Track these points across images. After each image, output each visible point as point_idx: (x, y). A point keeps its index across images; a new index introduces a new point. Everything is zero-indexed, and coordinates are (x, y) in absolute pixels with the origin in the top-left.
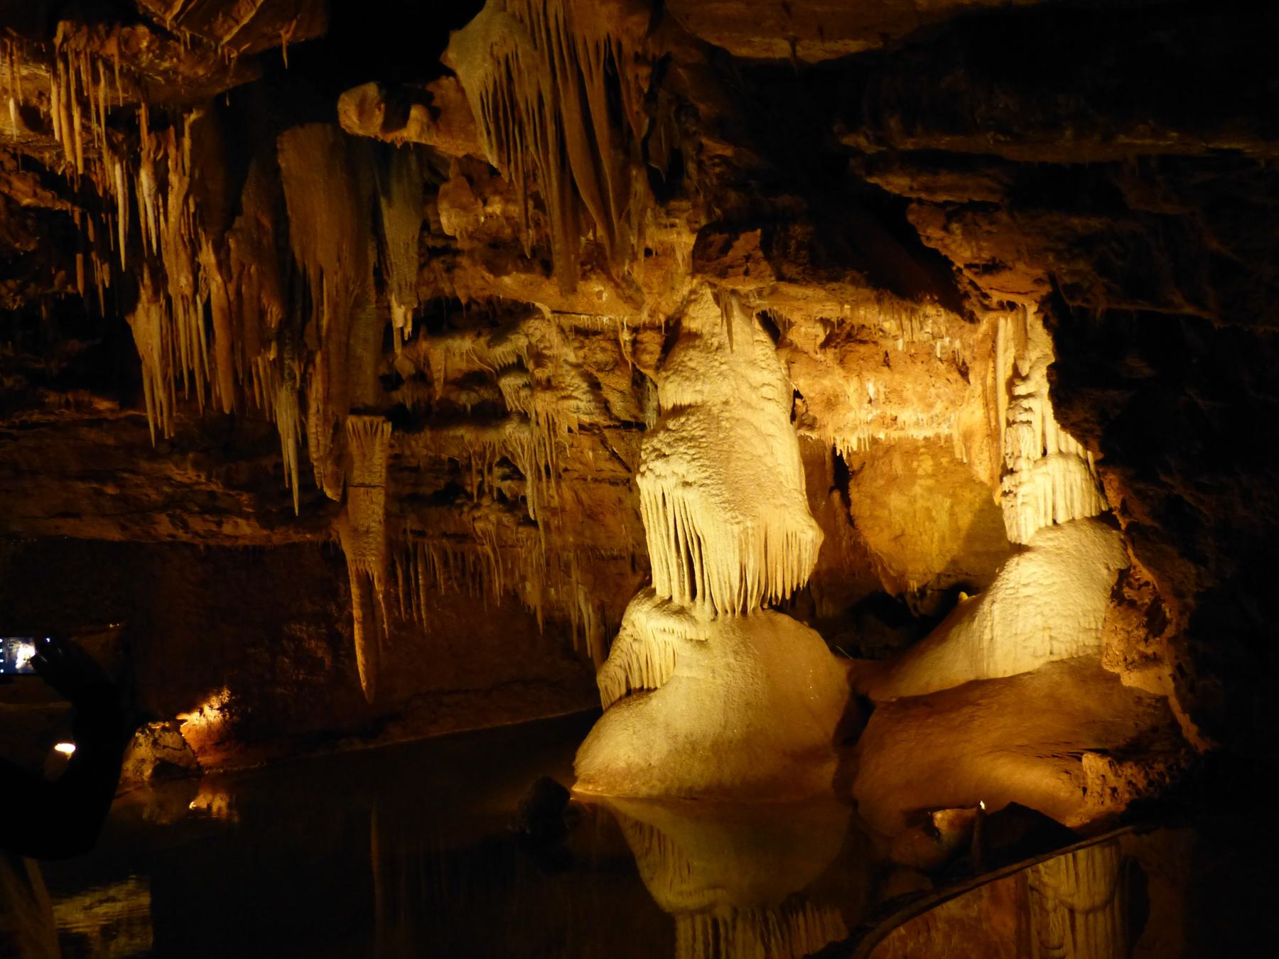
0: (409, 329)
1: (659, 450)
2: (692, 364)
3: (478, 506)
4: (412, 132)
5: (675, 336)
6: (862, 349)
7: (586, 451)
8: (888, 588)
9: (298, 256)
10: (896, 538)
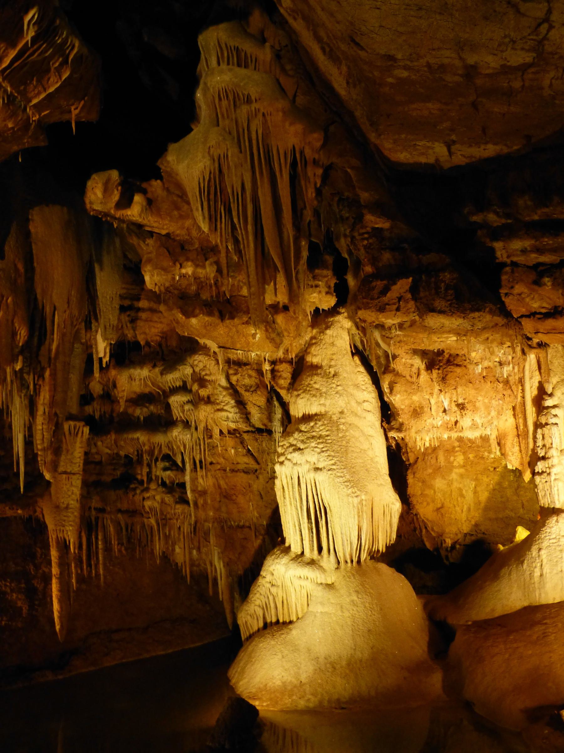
0: (107, 359)
1: (295, 445)
2: (316, 386)
3: (147, 489)
4: (135, 211)
5: (301, 369)
6: (458, 370)
7: (229, 449)
8: (428, 545)
9: (39, 297)
10: (438, 509)
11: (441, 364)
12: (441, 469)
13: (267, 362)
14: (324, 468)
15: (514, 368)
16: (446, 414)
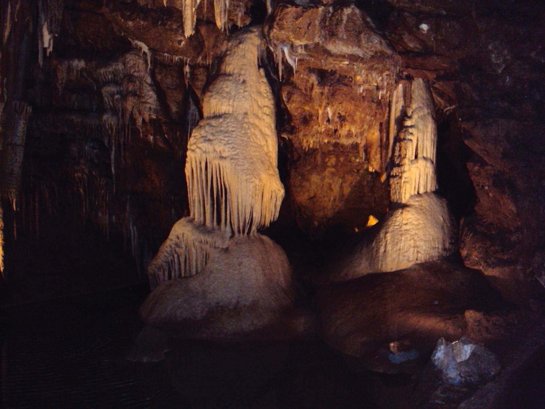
0: (51, 49)
2: (227, 90)
6: (345, 89)
10: (311, 198)
12: (318, 167)
14: (228, 157)
15: (387, 93)
16: (329, 124)
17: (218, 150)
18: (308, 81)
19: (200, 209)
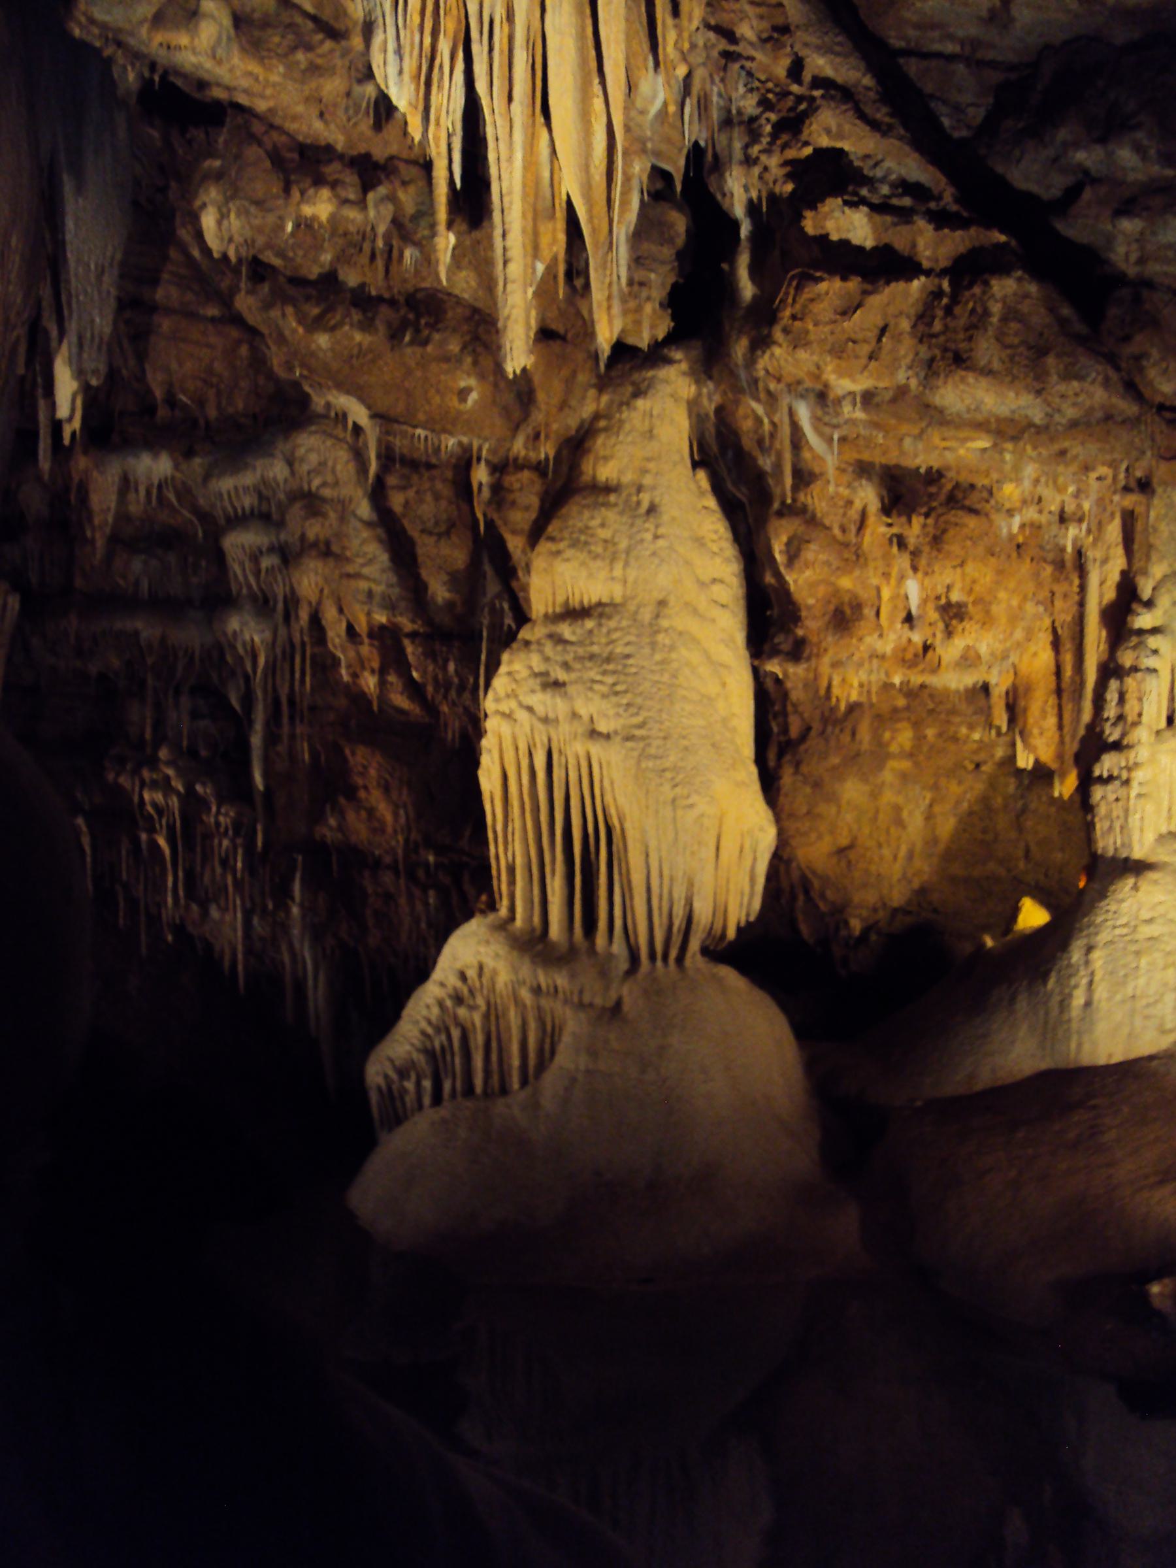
0: (77, 424)
6: (972, 522)
10: (841, 851)
11: (934, 504)
13: (483, 463)
14: (616, 733)
16: (912, 628)
17: (583, 711)
18: (850, 503)
19: (531, 890)
